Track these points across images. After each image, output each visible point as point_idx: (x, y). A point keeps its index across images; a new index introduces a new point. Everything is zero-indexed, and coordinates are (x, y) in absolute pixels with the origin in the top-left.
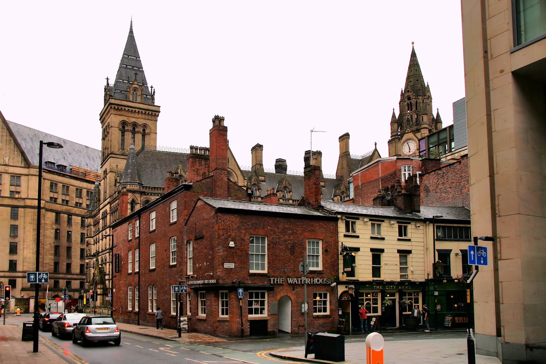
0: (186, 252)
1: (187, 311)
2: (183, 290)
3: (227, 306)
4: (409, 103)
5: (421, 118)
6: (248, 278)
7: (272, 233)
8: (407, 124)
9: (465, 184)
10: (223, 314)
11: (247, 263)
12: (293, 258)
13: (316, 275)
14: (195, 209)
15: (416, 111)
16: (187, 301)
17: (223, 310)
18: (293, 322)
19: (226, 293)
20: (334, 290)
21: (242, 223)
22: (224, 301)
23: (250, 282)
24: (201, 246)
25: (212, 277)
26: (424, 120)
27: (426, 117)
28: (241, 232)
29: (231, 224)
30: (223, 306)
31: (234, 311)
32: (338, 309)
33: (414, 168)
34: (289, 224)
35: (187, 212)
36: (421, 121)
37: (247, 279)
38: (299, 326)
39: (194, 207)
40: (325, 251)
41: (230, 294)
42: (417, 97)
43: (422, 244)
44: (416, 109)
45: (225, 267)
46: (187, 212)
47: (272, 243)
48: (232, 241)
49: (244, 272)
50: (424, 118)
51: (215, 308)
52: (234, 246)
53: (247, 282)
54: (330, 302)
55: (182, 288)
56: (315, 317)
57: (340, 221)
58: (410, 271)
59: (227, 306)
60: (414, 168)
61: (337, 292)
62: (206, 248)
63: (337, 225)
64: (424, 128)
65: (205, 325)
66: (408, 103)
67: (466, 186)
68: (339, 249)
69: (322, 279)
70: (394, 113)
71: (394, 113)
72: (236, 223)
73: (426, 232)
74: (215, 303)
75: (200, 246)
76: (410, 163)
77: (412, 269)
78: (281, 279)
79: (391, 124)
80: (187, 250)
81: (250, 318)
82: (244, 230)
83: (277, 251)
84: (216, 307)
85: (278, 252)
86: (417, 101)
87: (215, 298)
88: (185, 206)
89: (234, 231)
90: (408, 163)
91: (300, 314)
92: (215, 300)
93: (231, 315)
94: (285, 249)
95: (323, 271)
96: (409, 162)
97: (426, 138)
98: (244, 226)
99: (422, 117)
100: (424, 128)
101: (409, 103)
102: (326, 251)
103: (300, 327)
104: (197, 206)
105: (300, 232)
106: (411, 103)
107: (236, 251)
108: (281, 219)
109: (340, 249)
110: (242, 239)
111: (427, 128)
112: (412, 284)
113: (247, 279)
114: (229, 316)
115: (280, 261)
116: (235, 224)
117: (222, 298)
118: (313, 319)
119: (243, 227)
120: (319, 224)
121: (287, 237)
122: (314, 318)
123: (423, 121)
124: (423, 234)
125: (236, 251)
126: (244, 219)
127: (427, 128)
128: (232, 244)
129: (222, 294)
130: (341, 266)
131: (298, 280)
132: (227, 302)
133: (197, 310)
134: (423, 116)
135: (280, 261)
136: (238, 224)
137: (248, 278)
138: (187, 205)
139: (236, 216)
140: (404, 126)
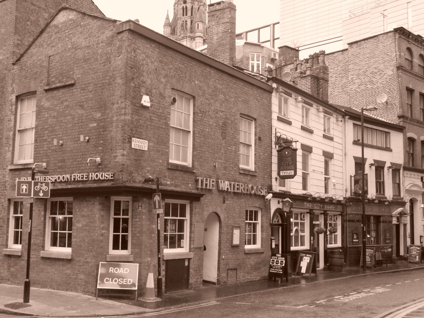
0: (13, 118)
1: (7, 240)
2: (39, 192)
3: (125, 230)
4: (185, 7)
5: (197, 25)
6: (167, 174)
7: (201, 94)
8: (182, 29)
9: (354, 79)
10: (116, 247)
11: (166, 143)
12: (224, 145)
13: (249, 178)
14: (48, 29)
15: (192, 17)
16: (8, 219)
17: (116, 238)
18: (221, 261)
19: (70, 204)
20: (266, 205)
21: (161, 62)
22: (120, 219)
23: (169, 183)
24: (65, 104)
25: (99, 167)
26: (199, 28)
27: (202, 25)
28: (159, 81)
29: (145, 60)
30: (116, 229)
31: (142, 242)
32: (271, 240)
33: (265, 59)
34: (221, 82)
35: (19, 40)
36: (197, 28)
37: (166, 177)
38: (228, 270)
39: (47, 25)
40: (259, 139)
41: (136, 204)
42: (193, 2)
43: (340, 147)
44: (192, 15)
45: (133, 146)
46: (19, 40)
47: (200, 111)
48: (147, 94)
49: (161, 161)
50: (199, 25)
51: (102, 235)
52: (149, 105)
53: (165, 182)
54: (262, 227)
55: (38, 187)
56: (247, 252)
57: (274, 94)
58: (332, 184)
59: (70, 229)
60: (265, 59)
61: (269, 211)
62: (82, 106)
63: (270, 98)
64: (199, 37)
65: (68, 272)
66: (183, 7)
67: (355, 82)
68: (273, 140)
69: (101, 174)
70: (168, 15)
71: (168, 15)
72: (153, 60)
73: (345, 130)
74: (103, 223)
75: (62, 103)
76: (260, 51)
77: (334, 181)
78: (211, 180)
79: (164, 26)
80: (16, 115)
81: (168, 255)
82: (164, 78)
83: (206, 129)
84: (104, 231)
85: (207, 130)
86: (192, 7)
87: (102, 213)
88: (16, 28)
89: (150, 76)
90: (258, 51)
91: (230, 246)
92: (102, 216)
93: (137, 250)
94: (216, 126)
95: (255, 172)
96: (258, 49)
97: (272, 26)
98: (163, 69)
99: (198, 24)
100: (199, 37)
101: (185, 7)
102: (260, 139)
103: (229, 271)
104: (55, 22)
105: (233, 99)
106: (186, 7)
107: (150, 117)
108: (212, 71)
109: (274, 140)
110: (161, 94)
111: (202, 37)
112: (331, 201)
113: (166, 177)
114: (132, 253)
115: (209, 147)
116: (152, 62)
117: (117, 213)
118: (244, 256)
119: (163, 72)
120: (253, 93)
121: (218, 105)
122: (246, 254)
123: (198, 29)
124: (342, 132)
125: (150, 117)
126: (165, 56)
127: (202, 37)
128: (146, 100)
129: (118, 204)
130: (275, 167)
131: (230, 185)
132: (126, 221)
133: (41, 238)
134: (199, 23)
135: (209, 147)
136: (155, 63)
137: (167, 174)
138: (18, 26)
139: (153, 46)
140: (178, 32)
